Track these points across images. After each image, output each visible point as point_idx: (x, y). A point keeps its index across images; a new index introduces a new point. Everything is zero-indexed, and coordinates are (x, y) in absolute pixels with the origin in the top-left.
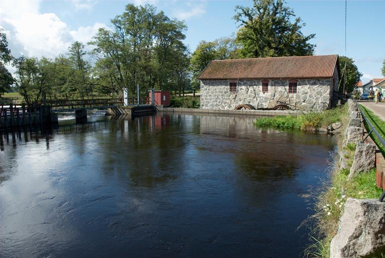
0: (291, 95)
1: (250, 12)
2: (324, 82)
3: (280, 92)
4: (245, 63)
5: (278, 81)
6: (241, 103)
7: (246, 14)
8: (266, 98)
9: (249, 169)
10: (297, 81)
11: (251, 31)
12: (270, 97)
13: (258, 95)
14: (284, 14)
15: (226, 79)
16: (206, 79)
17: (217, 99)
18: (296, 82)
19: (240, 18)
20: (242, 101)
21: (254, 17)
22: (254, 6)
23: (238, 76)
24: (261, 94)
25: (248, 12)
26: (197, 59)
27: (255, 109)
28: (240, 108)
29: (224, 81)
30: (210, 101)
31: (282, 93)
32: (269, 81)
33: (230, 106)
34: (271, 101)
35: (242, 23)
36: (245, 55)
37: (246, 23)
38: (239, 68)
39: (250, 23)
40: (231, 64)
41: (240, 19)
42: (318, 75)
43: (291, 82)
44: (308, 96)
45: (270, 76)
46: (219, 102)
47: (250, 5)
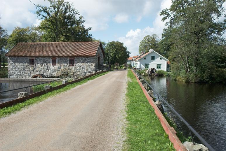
0: (71, 67)
1: (47, 10)
2: (91, 59)
3: (65, 66)
4: (41, 45)
5: (62, 59)
6: (38, 73)
7: (45, 11)
8: (55, 70)
9: (127, 132)
10: (74, 58)
11: (50, 23)
12: (57, 69)
13: (49, 67)
14: (72, 13)
15: (27, 57)
16: (12, 56)
17: (20, 70)
18: (73, 59)
19: (40, 13)
20: (39, 72)
21: (51, 13)
22: (51, 6)
23: (35, 55)
24: (51, 67)
25: (46, 9)
26: (13, 40)
27: (46, 77)
28: (35, 77)
29: (25, 57)
30: (15, 72)
31: (65, 66)
32: (56, 58)
33: (30, 76)
34: (58, 71)
35: (42, 17)
36: (46, 39)
37: (46, 17)
38: (36, 49)
39: (48, 17)
40: (31, 46)
41: (41, 14)
42: (87, 54)
43: (71, 59)
44: (81, 68)
45: (57, 55)
46: (22, 73)
47: (47, 4)
